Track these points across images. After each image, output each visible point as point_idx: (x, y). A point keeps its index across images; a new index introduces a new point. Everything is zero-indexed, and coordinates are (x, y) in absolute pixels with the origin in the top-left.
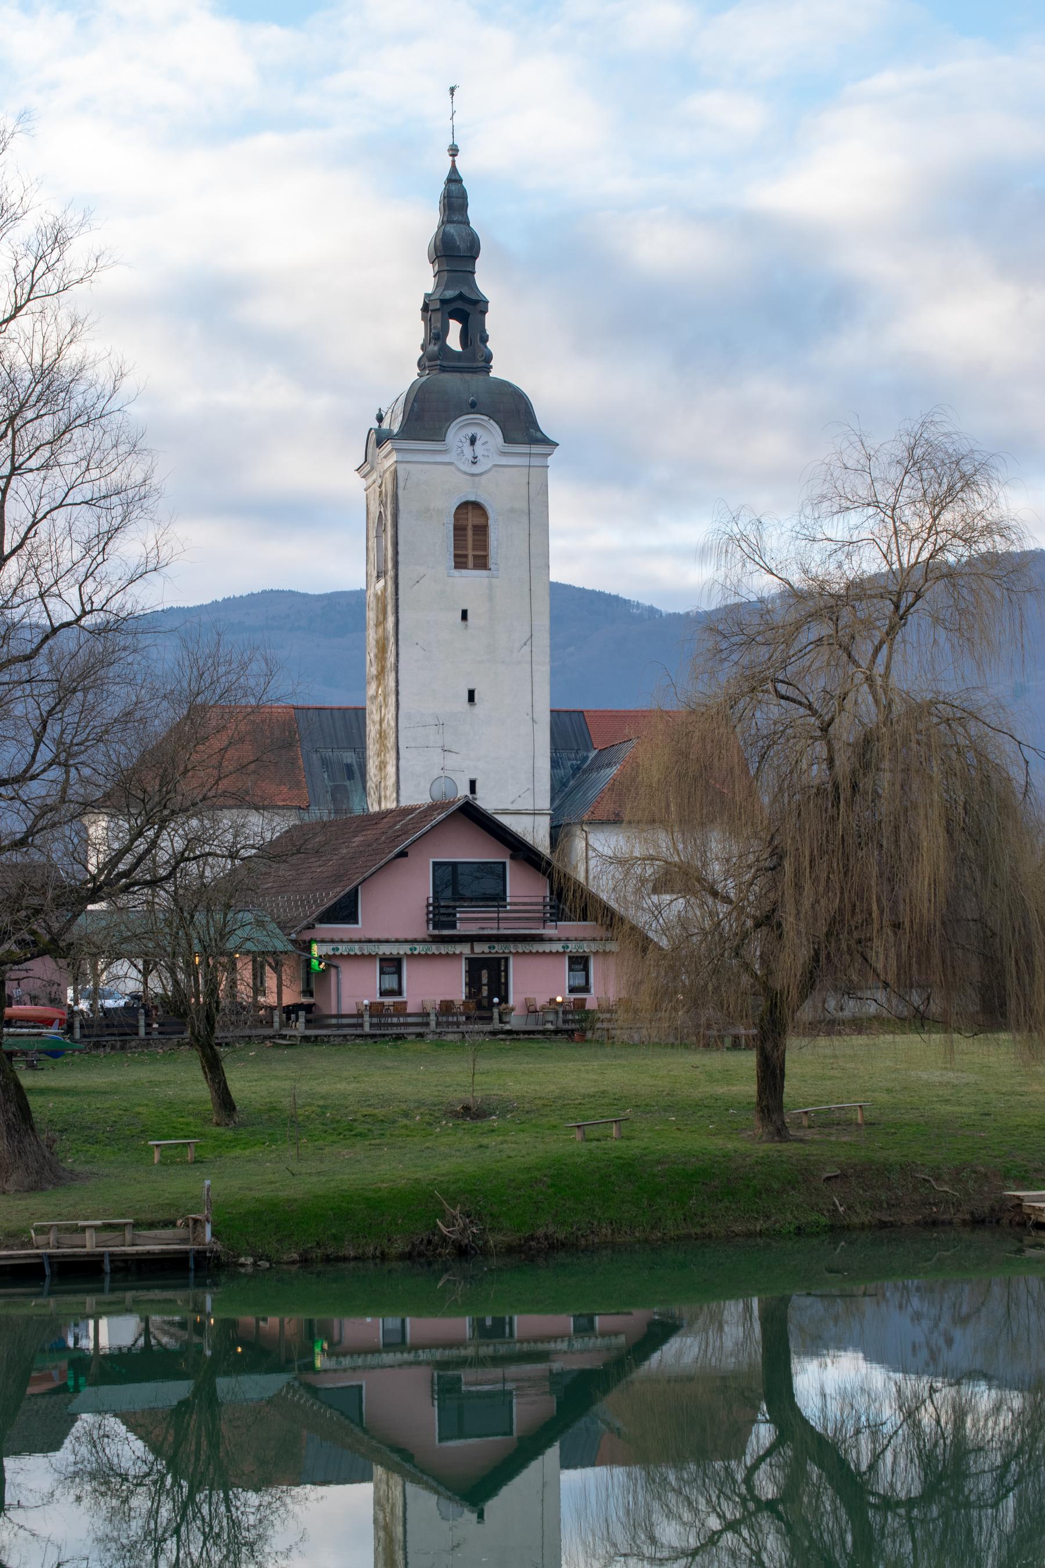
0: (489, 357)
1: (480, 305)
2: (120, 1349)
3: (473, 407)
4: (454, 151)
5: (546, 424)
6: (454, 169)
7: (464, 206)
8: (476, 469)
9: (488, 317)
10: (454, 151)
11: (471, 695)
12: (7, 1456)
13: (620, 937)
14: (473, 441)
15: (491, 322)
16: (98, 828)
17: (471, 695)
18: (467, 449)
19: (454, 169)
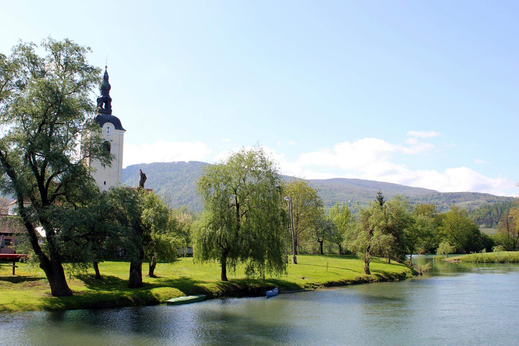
0: (111, 111)
1: (110, 100)
2: (360, 278)
3: (109, 121)
4: (106, 67)
5: (124, 126)
6: (106, 71)
7: (108, 78)
8: (108, 134)
9: (110, 91)
10: (106, 67)
11: (105, 182)
12: (126, 281)
13: (5, 208)
14: (108, 128)
15: (112, 104)
16: (37, 158)
17: (105, 182)
18: (107, 130)
19: (106, 71)
